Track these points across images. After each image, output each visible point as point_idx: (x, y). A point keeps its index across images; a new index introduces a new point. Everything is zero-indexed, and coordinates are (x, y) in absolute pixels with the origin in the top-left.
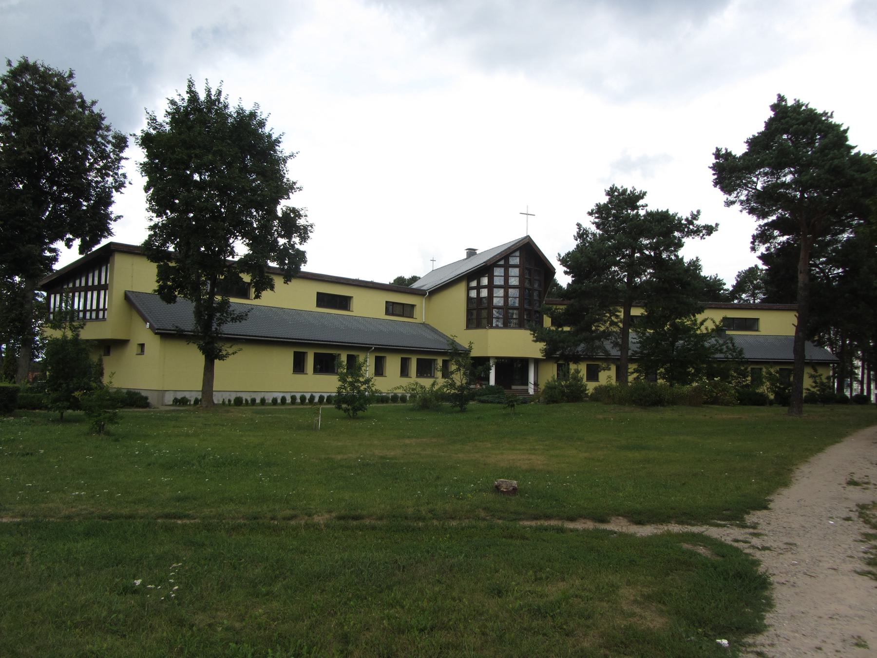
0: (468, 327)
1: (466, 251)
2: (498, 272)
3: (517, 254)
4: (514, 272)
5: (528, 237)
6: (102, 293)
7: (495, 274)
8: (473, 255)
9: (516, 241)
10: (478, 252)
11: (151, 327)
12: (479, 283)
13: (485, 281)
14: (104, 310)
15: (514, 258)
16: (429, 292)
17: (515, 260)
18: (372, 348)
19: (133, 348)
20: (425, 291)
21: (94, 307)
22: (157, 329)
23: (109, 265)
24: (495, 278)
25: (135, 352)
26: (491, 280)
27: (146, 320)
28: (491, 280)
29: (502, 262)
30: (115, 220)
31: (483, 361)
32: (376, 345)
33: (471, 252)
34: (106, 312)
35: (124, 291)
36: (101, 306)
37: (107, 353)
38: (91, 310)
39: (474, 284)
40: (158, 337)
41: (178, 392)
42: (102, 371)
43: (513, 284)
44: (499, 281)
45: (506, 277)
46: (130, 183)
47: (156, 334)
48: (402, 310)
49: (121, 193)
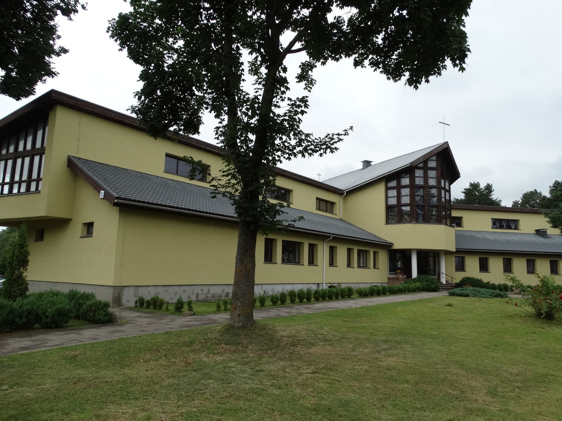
0: (387, 223)
1: (362, 163)
2: (419, 173)
3: (434, 158)
4: (432, 174)
5: (447, 143)
6: (37, 159)
7: (416, 175)
8: (369, 166)
9: (436, 147)
10: (372, 164)
11: (107, 197)
12: (399, 183)
13: (406, 181)
14: (38, 180)
15: (431, 162)
16: (346, 192)
17: (432, 164)
18: (330, 237)
19: (77, 229)
20: (343, 191)
21: (25, 178)
22: (117, 198)
23: (47, 128)
24: (416, 179)
25: (80, 235)
26: (412, 180)
27: (98, 188)
28: (412, 180)
29: (421, 165)
30: (58, 55)
31: (405, 254)
32: (333, 234)
33: (367, 164)
34: (41, 183)
35: (67, 156)
36: (35, 176)
37: (40, 237)
38: (20, 182)
39: (393, 184)
40: (117, 209)
41: (140, 289)
42: (26, 257)
43: (431, 184)
44: (419, 181)
45: (426, 178)
46: (83, 7)
47: (115, 204)
48: (325, 207)
49: (71, 19)
